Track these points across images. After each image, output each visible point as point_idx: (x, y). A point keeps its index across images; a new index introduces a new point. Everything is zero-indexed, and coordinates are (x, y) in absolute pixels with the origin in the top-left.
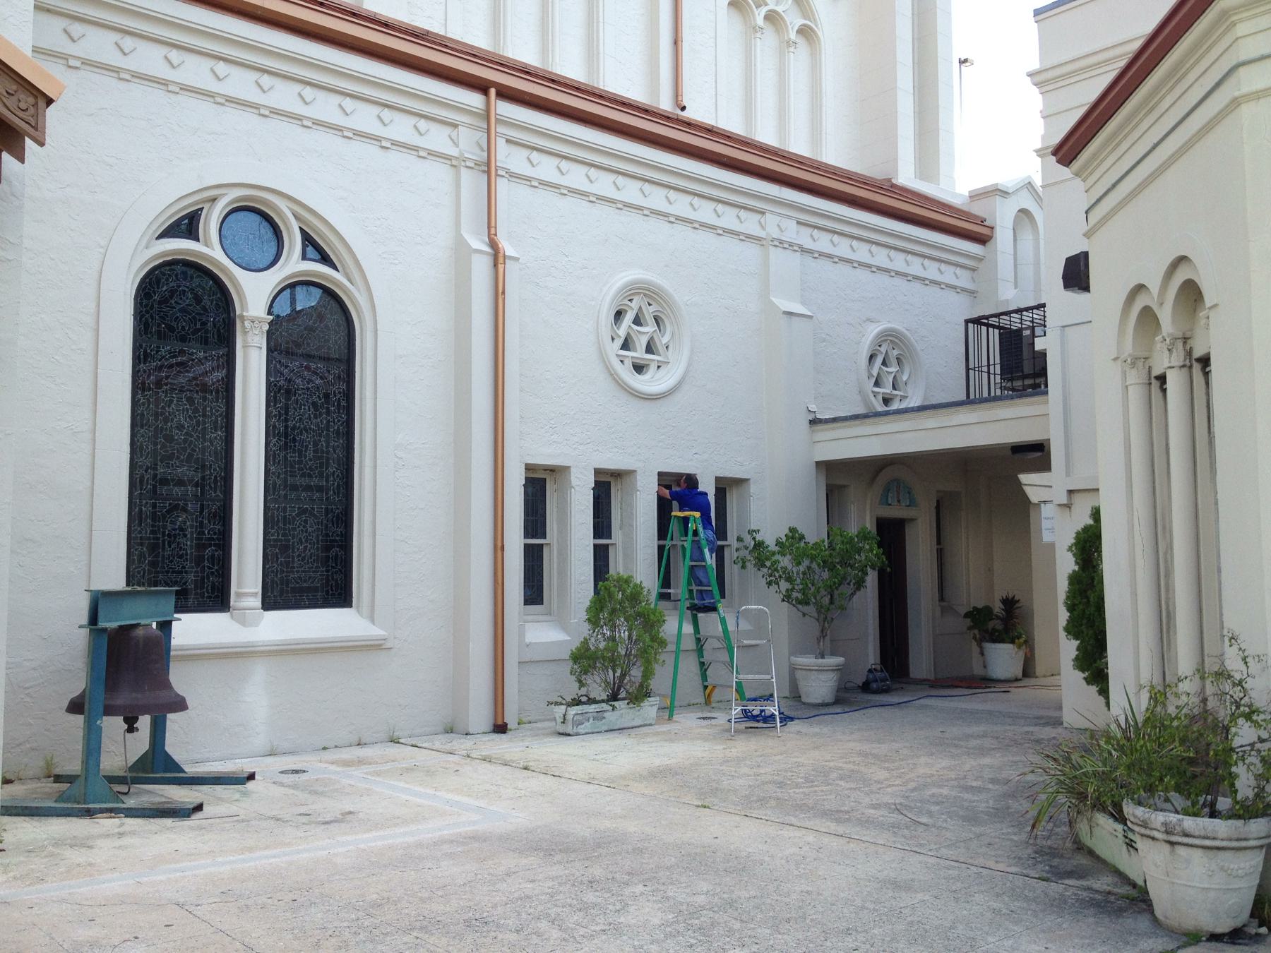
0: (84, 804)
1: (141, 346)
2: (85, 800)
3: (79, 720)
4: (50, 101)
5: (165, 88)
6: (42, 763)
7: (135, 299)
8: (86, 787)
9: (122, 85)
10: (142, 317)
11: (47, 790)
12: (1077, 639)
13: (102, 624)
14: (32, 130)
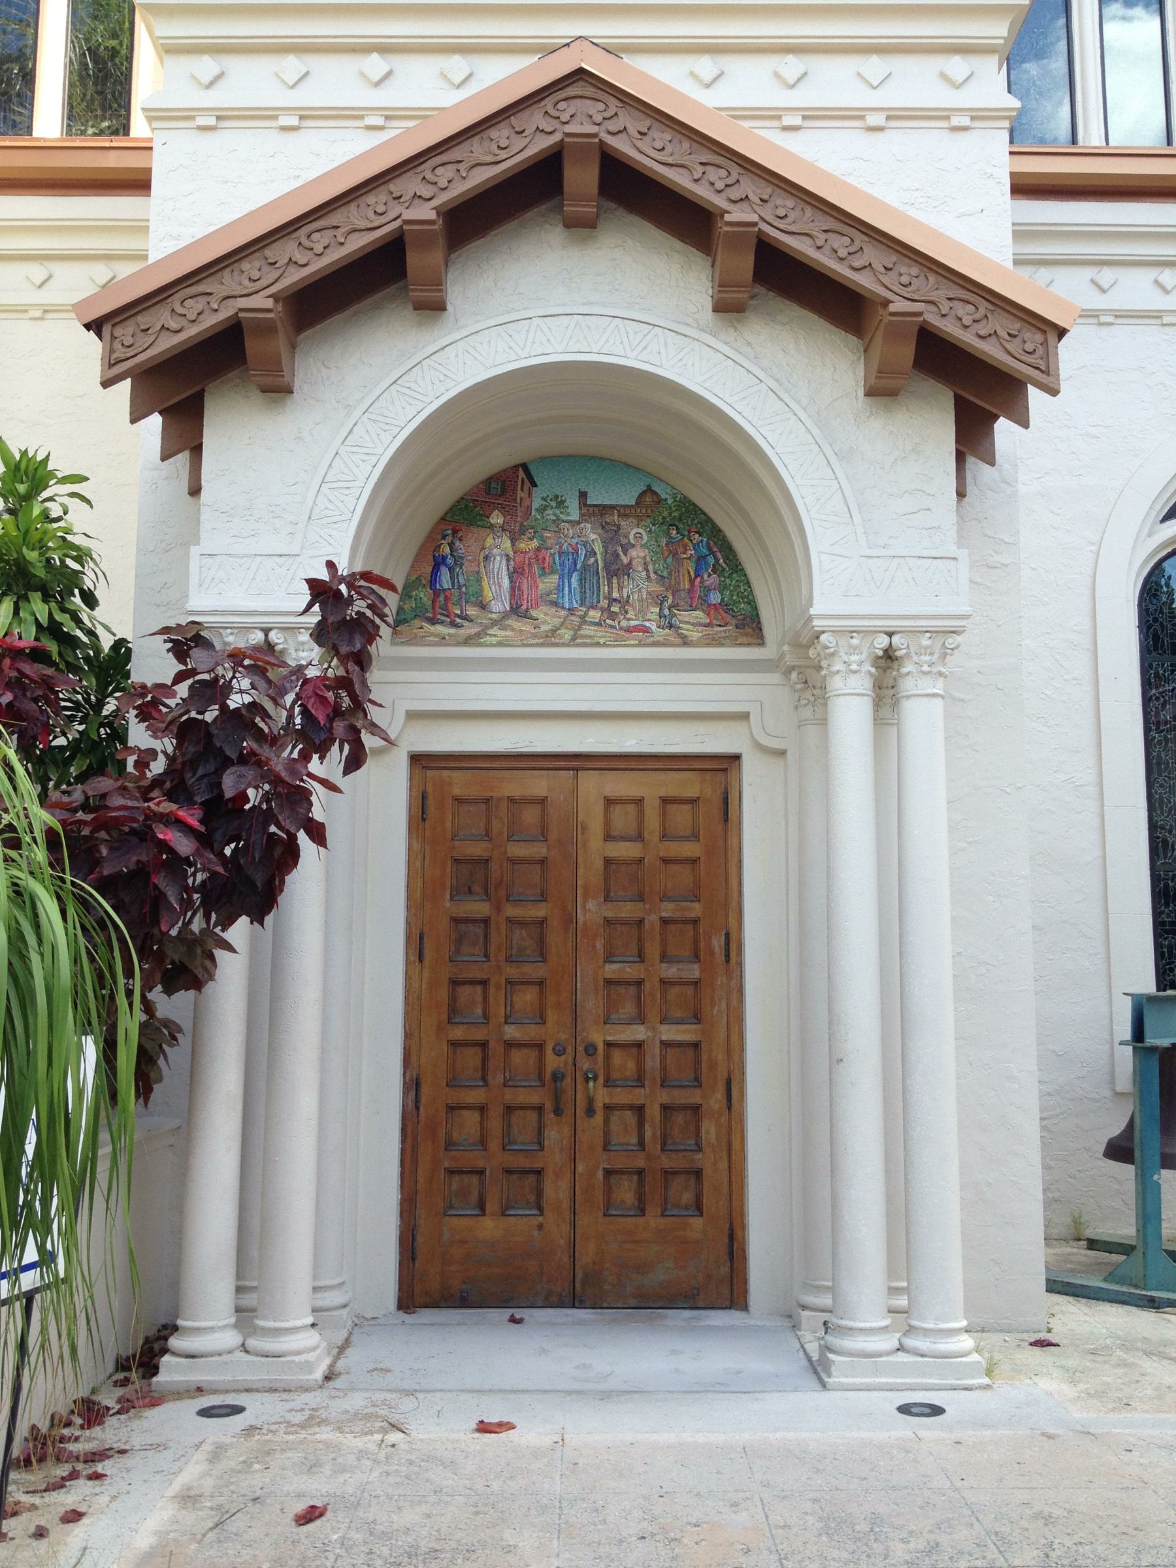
0: (1144, 1289)
1: (1151, 666)
2: (1145, 1285)
3: (1127, 1171)
4: (1061, 333)
5: (1158, 321)
6: (1069, 1220)
7: (1140, 605)
8: (1145, 1266)
9: (1105, 331)
10: (1149, 628)
11: (1082, 1259)
12: (200, 932)
13: (1150, 1041)
14: (1044, 376)
